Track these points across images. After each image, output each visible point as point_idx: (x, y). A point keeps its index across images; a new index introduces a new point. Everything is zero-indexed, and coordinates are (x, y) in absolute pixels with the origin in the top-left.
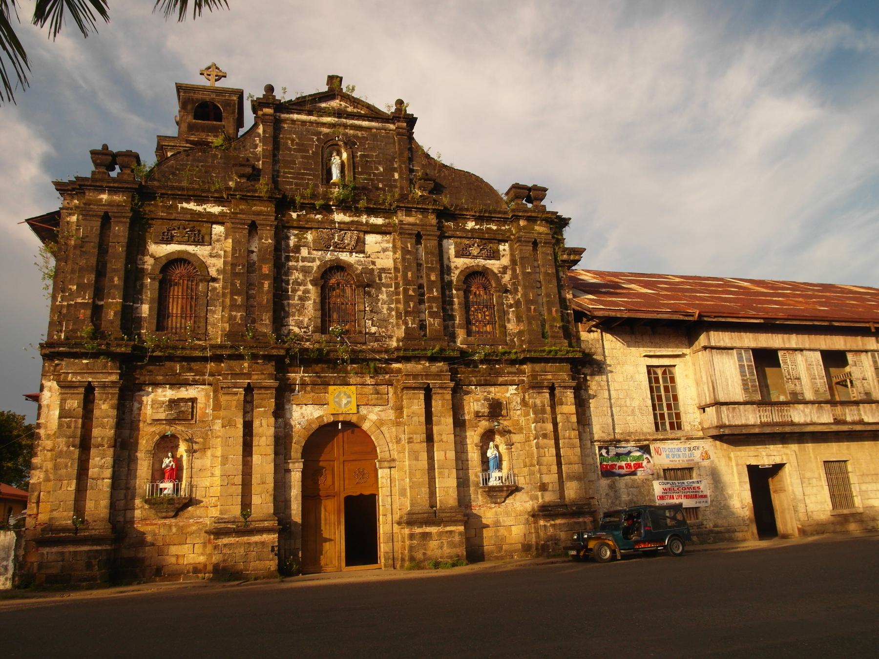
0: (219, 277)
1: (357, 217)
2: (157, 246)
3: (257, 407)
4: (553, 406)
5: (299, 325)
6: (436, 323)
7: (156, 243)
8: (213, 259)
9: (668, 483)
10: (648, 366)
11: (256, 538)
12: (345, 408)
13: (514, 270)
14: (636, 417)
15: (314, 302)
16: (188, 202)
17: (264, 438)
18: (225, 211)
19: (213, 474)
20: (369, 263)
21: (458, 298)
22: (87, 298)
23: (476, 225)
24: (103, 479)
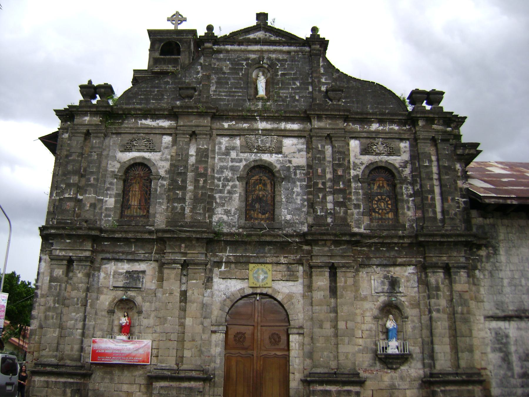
7: (121, 151)
8: (163, 162)
11: (186, 384)
15: (240, 195)
16: (146, 119)
17: (195, 304)
18: (173, 124)
24: (77, 329)
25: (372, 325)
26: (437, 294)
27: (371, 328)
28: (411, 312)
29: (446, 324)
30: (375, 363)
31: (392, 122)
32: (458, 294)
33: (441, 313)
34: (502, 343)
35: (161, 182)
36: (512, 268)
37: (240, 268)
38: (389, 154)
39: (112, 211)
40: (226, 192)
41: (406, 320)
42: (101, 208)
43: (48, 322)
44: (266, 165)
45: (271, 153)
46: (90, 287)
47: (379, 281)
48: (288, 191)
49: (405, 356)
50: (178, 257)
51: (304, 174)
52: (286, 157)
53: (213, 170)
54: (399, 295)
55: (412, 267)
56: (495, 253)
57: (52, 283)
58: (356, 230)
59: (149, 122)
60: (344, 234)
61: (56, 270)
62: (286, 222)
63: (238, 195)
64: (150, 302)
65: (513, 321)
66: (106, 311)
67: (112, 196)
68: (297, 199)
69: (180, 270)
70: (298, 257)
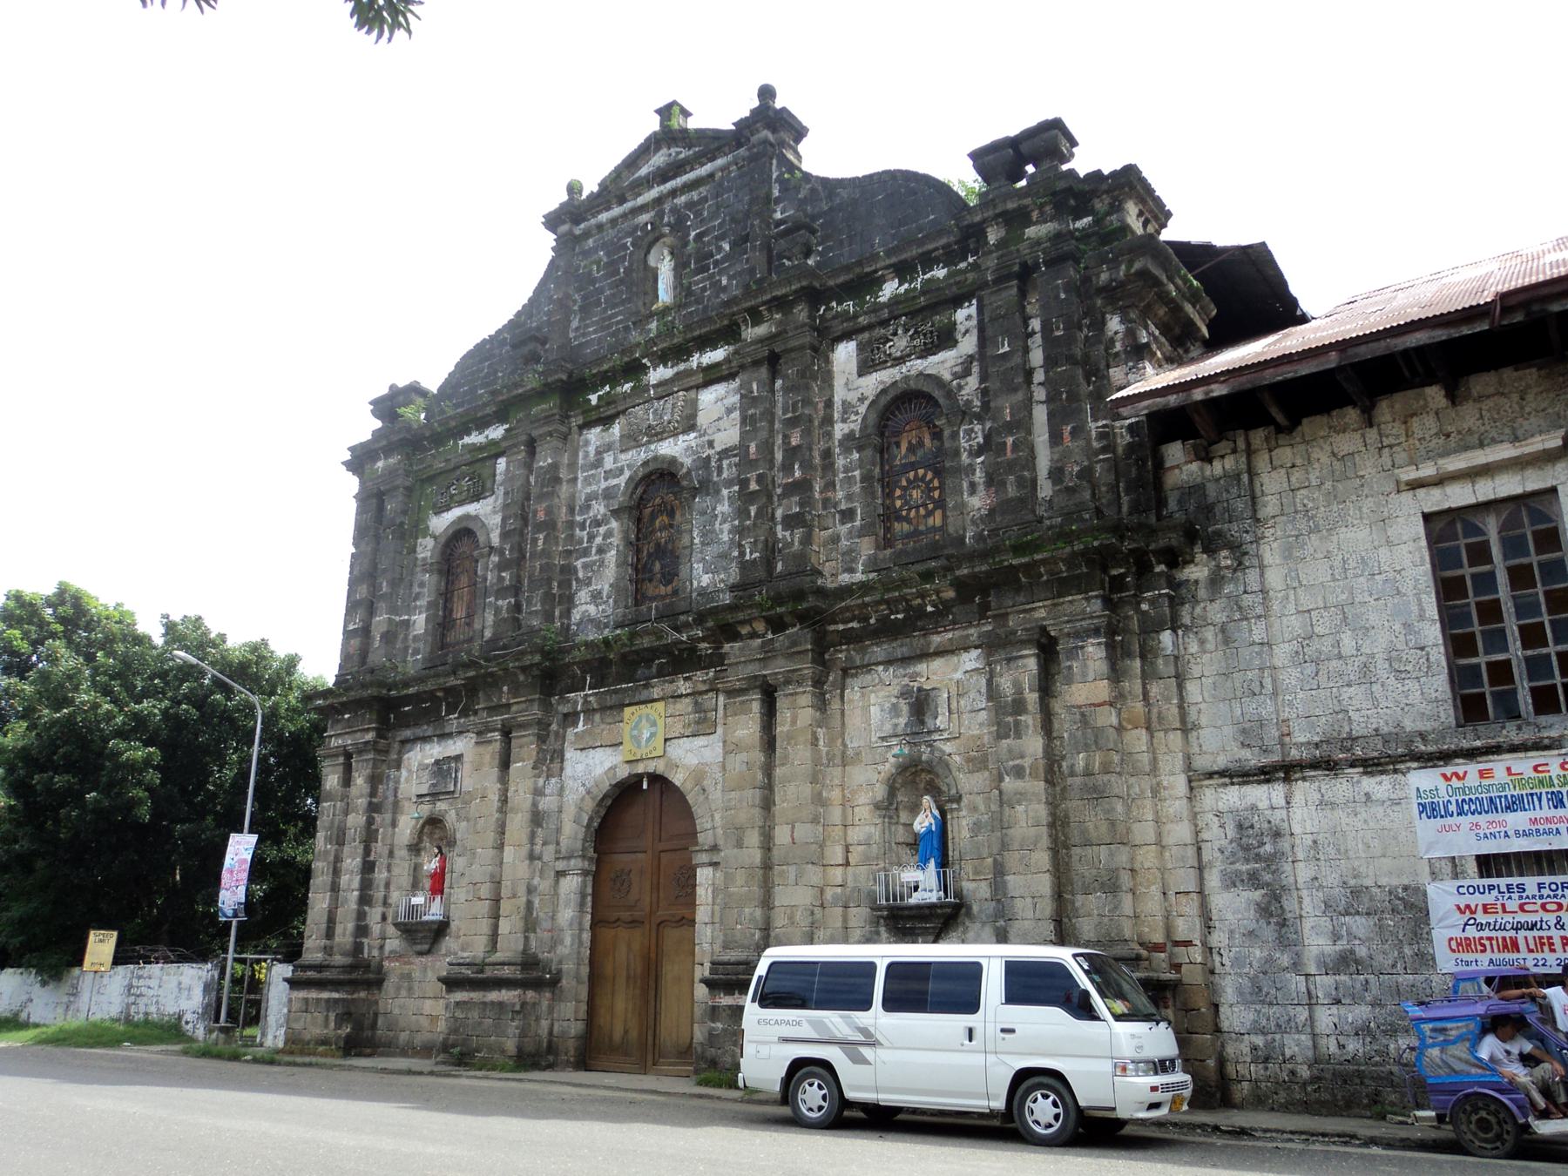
1: (685, 361)
4: (1046, 687)
6: (796, 540)
9: (1491, 888)
10: (1427, 518)
11: (493, 996)
14: (1375, 687)
17: (520, 815)
23: (900, 284)
25: (873, 829)
26: (1017, 723)
27: (870, 837)
28: (969, 783)
29: (1041, 811)
30: (878, 933)
32: (1078, 716)
33: (1027, 778)
34: (1258, 858)
36: (1306, 601)
41: (955, 806)
42: (406, 638)
45: (675, 434)
46: (917, 789)
47: (887, 705)
48: (706, 517)
49: (939, 911)
53: (571, 510)
54: (936, 736)
55: (975, 653)
56: (1240, 564)
58: (845, 578)
59: (474, 438)
62: (699, 595)
65: (1304, 779)
68: (722, 531)
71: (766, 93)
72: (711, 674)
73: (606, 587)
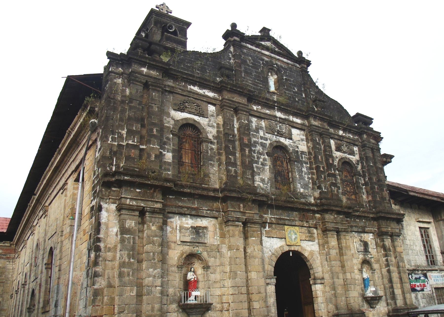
0: (214, 141)
2: (175, 112)
3: (251, 237)
5: (263, 181)
7: (174, 110)
8: (210, 128)
12: (294, 241)
13: (362, 163)
15: (270, 167)
16: (194, 86)
17: (257, 259)
18: (216, 96)
19: (224, 286)
20: (295, 147)
21: (340, 176)
22: (136, 141)
24: (156, 286)
31: (350, 132)
35: (210, 145)
37: (278, 229)
38: (350, 154)
39: (170, 165)
40: (260, 163)
43: (124, 280)
44: (284, 146)
50: (239, 215)
51: (307, 158)
52: (295, 143)
55: (372, 234)
57: (125, 236)
60: (336, 206)
61: (128, 221)
63: (268, 167)
64: (215, 258)
66: (176, 266)
67: (169, 151)
69: (242, 228)
70: (314, 222)
71: (234, 26)
72: (314, 222)
73: (266, 179)
